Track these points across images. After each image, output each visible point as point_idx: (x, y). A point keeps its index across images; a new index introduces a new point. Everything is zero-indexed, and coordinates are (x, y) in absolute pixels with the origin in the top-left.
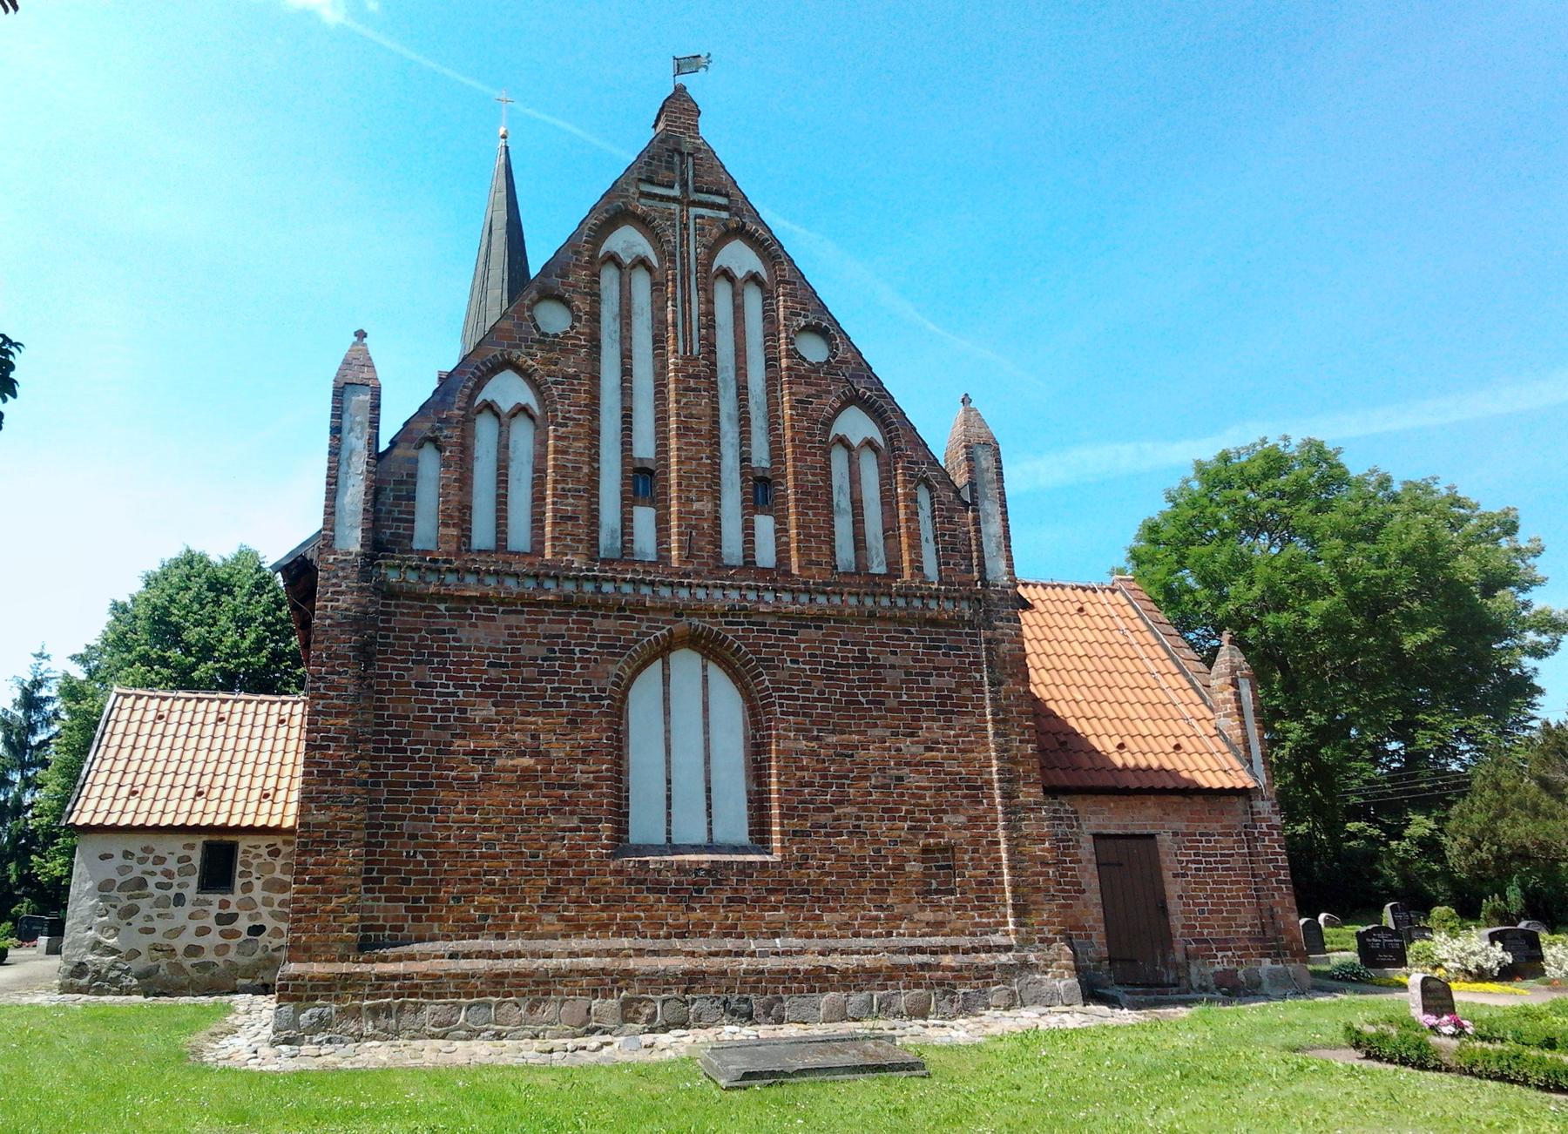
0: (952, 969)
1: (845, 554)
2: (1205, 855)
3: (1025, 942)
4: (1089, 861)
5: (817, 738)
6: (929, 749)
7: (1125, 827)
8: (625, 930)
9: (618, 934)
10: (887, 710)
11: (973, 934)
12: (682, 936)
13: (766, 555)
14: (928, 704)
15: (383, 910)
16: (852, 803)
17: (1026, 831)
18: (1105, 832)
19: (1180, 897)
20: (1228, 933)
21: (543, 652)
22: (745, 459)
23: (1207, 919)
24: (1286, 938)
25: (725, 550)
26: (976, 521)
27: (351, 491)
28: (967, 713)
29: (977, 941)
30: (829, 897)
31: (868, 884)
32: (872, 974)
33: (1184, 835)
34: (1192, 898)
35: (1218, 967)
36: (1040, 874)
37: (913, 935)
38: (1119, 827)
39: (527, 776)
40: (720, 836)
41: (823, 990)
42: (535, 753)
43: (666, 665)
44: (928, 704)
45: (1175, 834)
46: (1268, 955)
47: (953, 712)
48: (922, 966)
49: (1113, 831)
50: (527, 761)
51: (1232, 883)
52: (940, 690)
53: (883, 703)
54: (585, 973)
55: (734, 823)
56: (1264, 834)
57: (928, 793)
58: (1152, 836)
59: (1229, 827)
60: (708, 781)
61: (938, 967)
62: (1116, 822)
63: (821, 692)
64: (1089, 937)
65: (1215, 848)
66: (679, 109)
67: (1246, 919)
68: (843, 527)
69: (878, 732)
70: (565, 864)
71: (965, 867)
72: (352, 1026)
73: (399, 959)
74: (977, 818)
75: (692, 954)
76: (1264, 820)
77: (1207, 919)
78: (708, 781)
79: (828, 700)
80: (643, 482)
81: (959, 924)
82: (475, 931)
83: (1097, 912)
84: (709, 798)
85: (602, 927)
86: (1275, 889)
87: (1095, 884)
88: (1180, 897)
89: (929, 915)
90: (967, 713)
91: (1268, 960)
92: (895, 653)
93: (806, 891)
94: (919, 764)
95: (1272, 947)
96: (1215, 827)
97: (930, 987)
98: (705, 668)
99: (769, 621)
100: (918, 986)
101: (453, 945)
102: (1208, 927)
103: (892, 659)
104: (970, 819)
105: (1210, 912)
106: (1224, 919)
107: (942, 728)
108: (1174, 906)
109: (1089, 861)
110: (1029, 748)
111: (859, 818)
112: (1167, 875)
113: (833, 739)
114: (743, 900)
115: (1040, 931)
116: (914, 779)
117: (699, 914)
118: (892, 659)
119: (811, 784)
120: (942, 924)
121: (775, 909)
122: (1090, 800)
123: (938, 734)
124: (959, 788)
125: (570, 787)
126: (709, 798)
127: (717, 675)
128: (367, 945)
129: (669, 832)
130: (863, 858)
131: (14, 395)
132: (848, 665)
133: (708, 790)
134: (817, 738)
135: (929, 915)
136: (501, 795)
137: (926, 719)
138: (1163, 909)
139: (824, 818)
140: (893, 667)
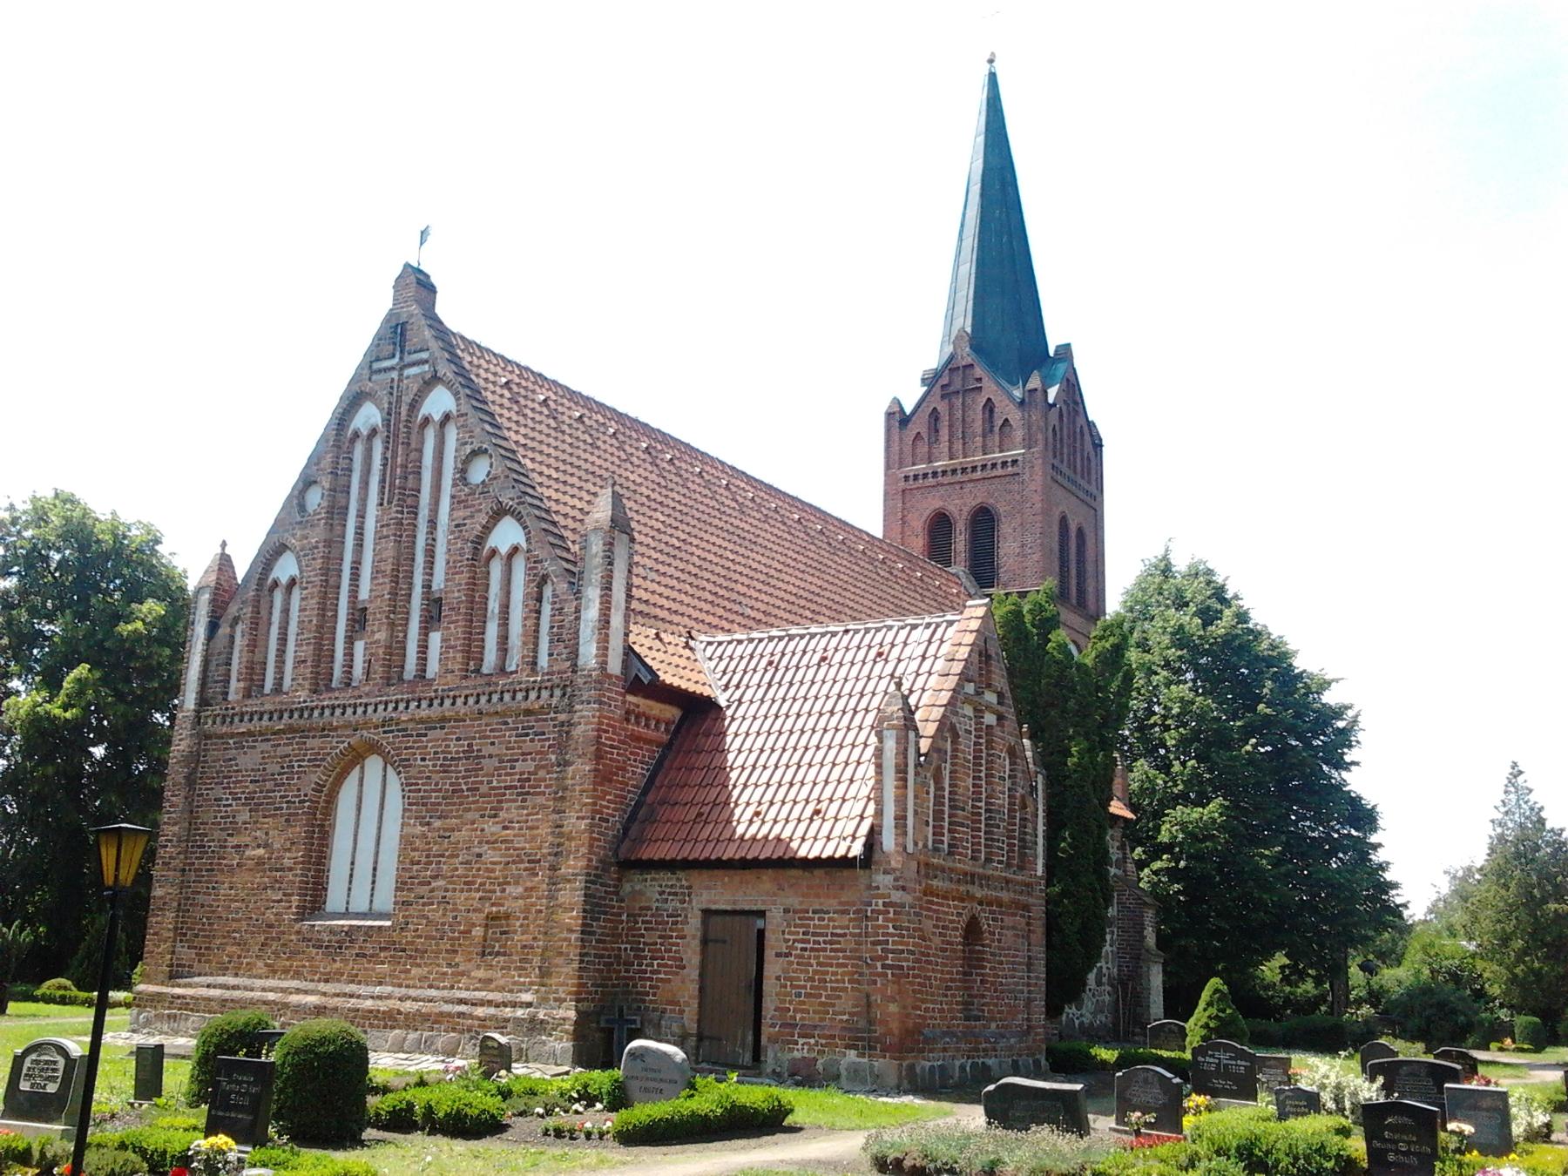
0: (479, 1018)
2: (814, 934)
3: (543, 1001)
4: (694, 937)
5: (428, 824)
6: (505, 828)
8: (297, 975)
9: (293, 978)
11: (511, 991)
12: (327, 981)
14: (511, 787)
15: (186, 953)
16: (444, 877)
17: (561, 900)
18: (714, 907)
19: (778, 978)
20: (822, 1020)
21: (277, 769)
22: (427, 586)
23: (804, 1003)
24: (880, 1030)
26: (578, 610)
27: (589, 631)
28: (539, 794)
29: (509, 997)
30: (418, 955)
31: (445, 945)
32: (425, 1017)
33: (795, 912)
34: (791, 979)
35: (797, 1054)
36: (565, 939)
37: (467, 989)
38: (727, 902)
39: (260, 862)
40: (377, 906)
41: (393, 1028)
42: (266, 846)
44: (511, 787)
45: (786, 911)
46: (855, 1047)
47: (528, 793)
48: (460, 1015)
50: (261, 851)
51: (838, 965)
52: (522, 773)
54: (265, 1003)
55: (386, 898)
56: (879, 912)
57: (498, 867)
59: (847, 903)
60: (376, 862)
61: (471, 1016)
62: (728, 897)
64: (682, 1012)
65: (827, 927)
66: (417, 286)
67: (846, 1005)
68: (492, 631)
69: (469, 816)
70: (271, 926)
71: (515, 932)
72: (159, 1025)
73: (185, 986)
74: (532, 889)
75: (324, 994)
76: (882, 896)
77: (804, 1003)
78: (376, 862)
81: (502, 982)
82: (223, 970)
83: (693, 988)
85: (286, 971)
86: (879, 975)
87: (696, 960)
88: (778, 978)
89: (481, 974)
90: (539, 794)
91: (853, 1052)
92: (493, 744)
93: (404, 950)
94: (495, 842)
95: (862, 1039)
96: (833, 904)
97: (462, 1032)
98: (385, 769)
99: (410, 726)
100: (454, 1030)
101: (210, 980)
102: (803, 1011)
105: (808, 995)
107: (518, 808)
109: (694, 937)
110: (583, 825)
111: (447, 890)
113: (437, 824)
114: (364, 956)
115: (556, 992)
116: (491, 856)
117: (338, 965)
119: (418, 863)
120: (490, 981)
121: (383, 963)
122: (706, 874)
123: (514, 814)
124: (522, 862)
125: (282, 870)
128: (173, 976)
130: (443, 924)
133: (375, 869)
134: (428, 824)
135: (481, 974)
136: (247, 877)
139: (423, 890)
140: (490, 756)
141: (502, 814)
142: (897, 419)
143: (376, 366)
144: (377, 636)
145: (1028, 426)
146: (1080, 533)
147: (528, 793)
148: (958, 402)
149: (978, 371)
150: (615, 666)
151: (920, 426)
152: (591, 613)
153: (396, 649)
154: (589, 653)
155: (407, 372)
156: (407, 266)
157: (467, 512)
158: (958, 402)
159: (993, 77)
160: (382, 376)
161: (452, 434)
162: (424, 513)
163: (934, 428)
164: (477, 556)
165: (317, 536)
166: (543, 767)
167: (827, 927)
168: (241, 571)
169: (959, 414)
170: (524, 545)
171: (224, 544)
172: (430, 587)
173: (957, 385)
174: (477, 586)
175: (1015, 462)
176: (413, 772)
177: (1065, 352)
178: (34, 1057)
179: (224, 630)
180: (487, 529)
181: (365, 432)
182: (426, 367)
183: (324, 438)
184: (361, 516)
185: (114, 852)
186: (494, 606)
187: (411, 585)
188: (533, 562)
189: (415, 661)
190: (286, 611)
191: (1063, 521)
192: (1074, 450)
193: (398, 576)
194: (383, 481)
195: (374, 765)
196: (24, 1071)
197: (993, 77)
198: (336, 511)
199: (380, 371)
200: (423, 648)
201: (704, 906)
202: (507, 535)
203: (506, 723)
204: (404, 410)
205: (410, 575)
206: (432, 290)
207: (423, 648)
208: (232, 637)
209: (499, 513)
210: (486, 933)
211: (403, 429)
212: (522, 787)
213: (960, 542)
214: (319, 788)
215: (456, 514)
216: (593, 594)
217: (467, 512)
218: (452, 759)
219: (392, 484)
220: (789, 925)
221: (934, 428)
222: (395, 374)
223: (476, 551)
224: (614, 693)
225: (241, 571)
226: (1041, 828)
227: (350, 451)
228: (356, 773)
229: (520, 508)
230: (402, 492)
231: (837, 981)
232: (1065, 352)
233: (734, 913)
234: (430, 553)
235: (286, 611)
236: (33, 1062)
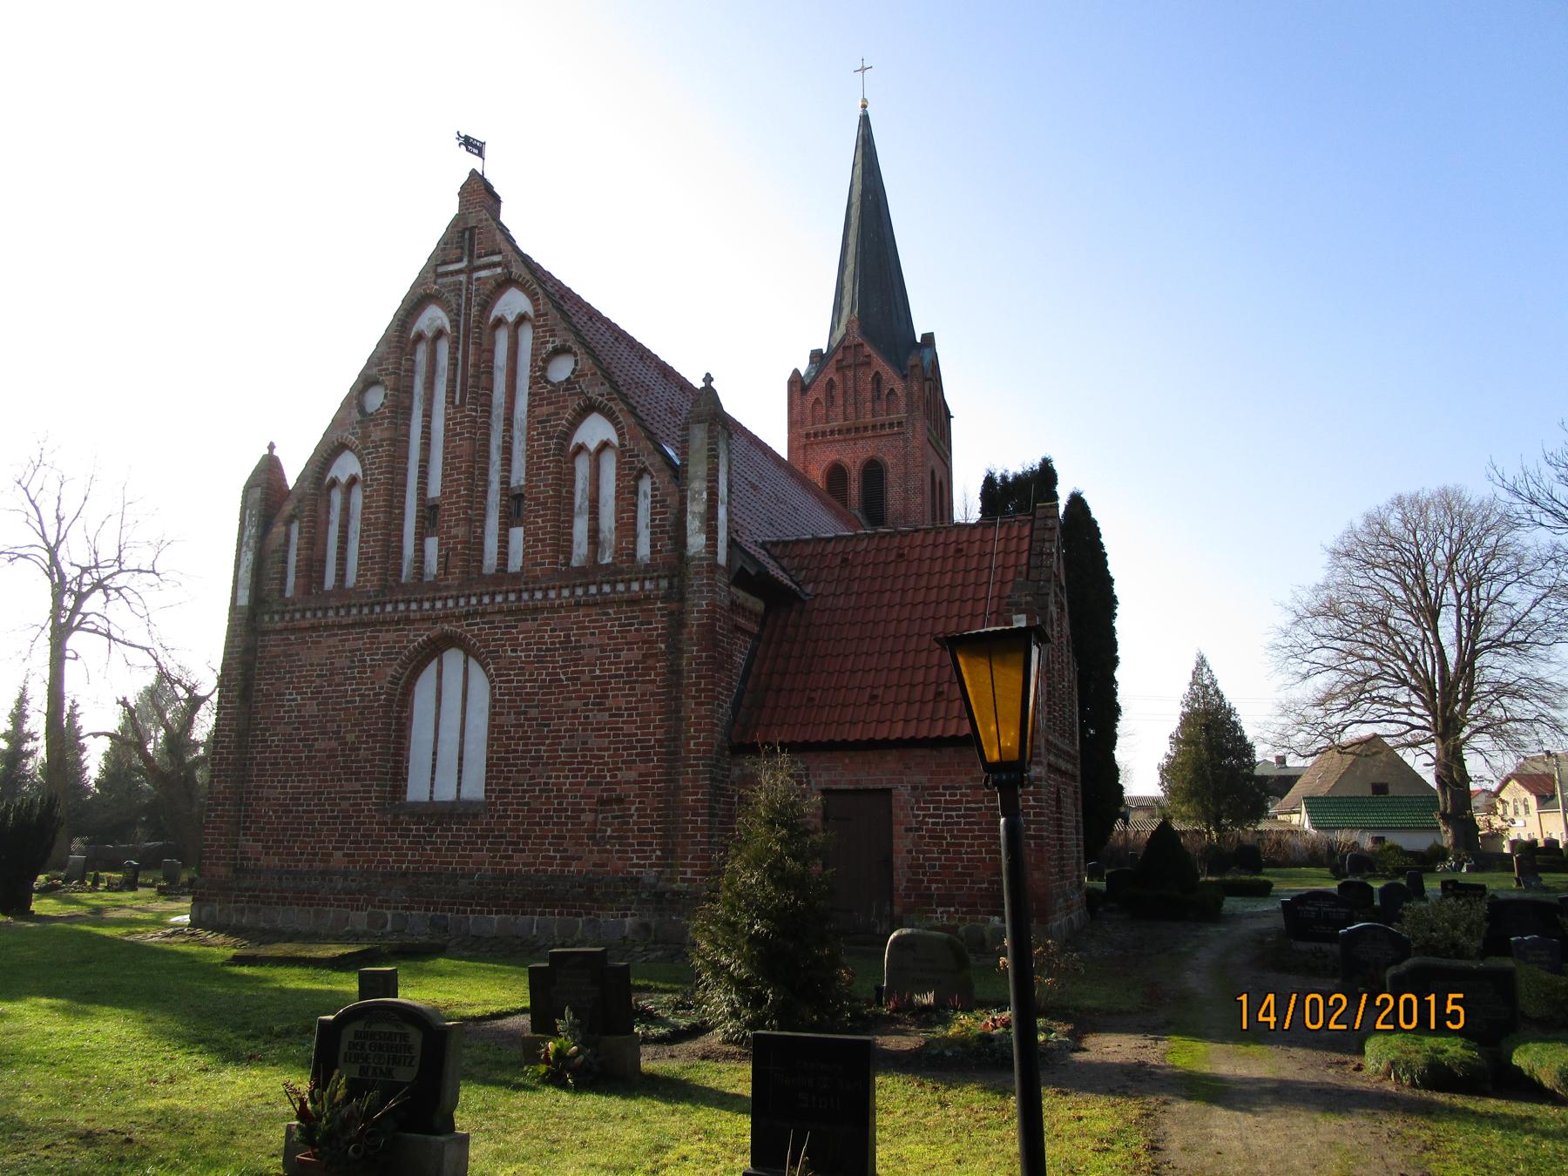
1: (580, 549)
2: (946, 809)
7: (858, 782)
10: (583, 685)
13: (516, 563)
19: (909, 852)
21: (347, 663)
22: (505, 481)
25: (510, 563)
34: (924, 852)
43: (440, 663)
44: (616, 676)
45: (914, 788)
47: (636, 682)
49: (843, 786)
51: (974, 838)
52: (628, 662)
53: (578, 679)
58: (889, 791)
63: (531, 674)
65: (960, 802)
66: (479, 196)
68: (581, 527)
79: (535, 681)
80: (430, 516)
84: (434, 760)
92: (593, 634)
98: (466, 662)
99: (497, 618)
102: (936, 882)
103: (591, 640)
104: (640, 775)
106: (958, 874)
108: (900, 860)
112: (898, 830)
118: (591, 640)
126: (434, 760)
127: (475, 667)
129: (459, 791)
131: (1045, 475)
132: (556, 649)
137: (613, 689)
138: (887, 860)
140: (591, 646)
141: (608, 703)
142: (266, 494)
143: (441, 269)
144: (454, 532)
145: (909, 395)
147: (636, 682)
148: (850, 374)
149: (868, 349)
150: (722, 558)
151: (817, 393)
152: (696, 508)
154: (696, 541)
155: (476, 275)
157: (552, 408)
158: (850, 374)
159: (865, 121)
160: (449, 279)
161: (526, 337)
162: (498, 411)
163: (830, 398)
164: (557, 453)
166: (652, 655)
167: (960, 802)
168: (292, 473)
169: (850, 384)
170: (615, 440)
171: (271, 447)
172: (508, 483)
173: (850, 361)
175: (900, 424)
176: (503, 663)
177: (929, 339)
178: (359, 1026)
179: (278, 530)
180: (574, 425)
181: (429, 334)
182: (499, 270)
183: (385, 340)
184: (428, 415)
186: (580, 499)
187: (487, 483)
188: (622, 452)
189: (495, 556)
190: (346, 509)
193: (469, 464)
194: (451, 382)
195: (453, 660)
196: (344, 1048)
197: (865, 121)
198: (399, 410)
199: (446, 274)
200: (504, 542)
201: (823, 786)
202: (595, 431)
203: (608, 614)
204: (474, 311)
205: (485, 472)
206: (497, 200)
207: (504, 542)
208: (288, 536)
209: (588, 408)
210: (1500, 789)
211: (475, 332)
212: (630, 675)
213: (854, 489)
214: (395, 680)
215: (538, 411)
216: (698, 486)
217: (552, 408)
218: (548, 650)
219: (464, 384)
220: (918, 802)
221: (830, 398)
222: (463, 278)
223: (562, 448)
224: (722, 580)
225: (292, 473)
227: (413, 353)
228: (432, 668)
229: (611, 404)
230: (473, 389)
231: (974, 852)
232: (929, 339)
233: (857, 792)
234: (507, 450)
235: (346, 509)
236: (357, 1034)
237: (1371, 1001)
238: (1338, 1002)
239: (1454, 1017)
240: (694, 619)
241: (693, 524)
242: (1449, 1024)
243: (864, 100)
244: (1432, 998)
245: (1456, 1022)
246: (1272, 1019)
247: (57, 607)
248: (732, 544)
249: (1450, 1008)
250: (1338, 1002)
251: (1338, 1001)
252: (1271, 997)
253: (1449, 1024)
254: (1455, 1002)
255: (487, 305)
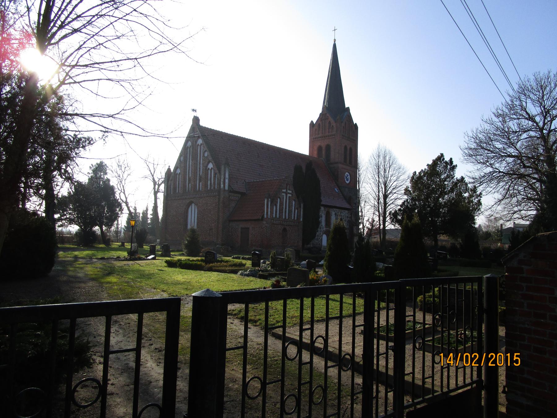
22: (199, 174)
66: (196, 120)
142: (312, 125)
146: (351, 149)
152: (222, 180)
153: (196, 185)
156: (194, 116)
165: (182, 165)
174: (207, 174)
177: (348, 108)
179: (170, 182)
185: (270, 352)
191: (346, 147)
192: (351, 130)
193: (195, 173)
195: (193, 205)
223: (206, 169)
226: (302, 213)
230: (195, 158)
232: (348, 108)
234: (200, 169)
237: (487, 356)
238: (475, 356)
239: (517, 361)
240: (221, 199)
241: (222, 183)
242: (515, 364)
243: (135, 207)
244: (509, 355)
245: (517, 363)
246: (452, 362)
247: (154, 188)
248: (229, 186)
249: (515, 358)
250: (475, 356)
251: (475, 356)
252: (451, 354)
253: (515, 364)
254: (517, 356)
255: (196, 142)
